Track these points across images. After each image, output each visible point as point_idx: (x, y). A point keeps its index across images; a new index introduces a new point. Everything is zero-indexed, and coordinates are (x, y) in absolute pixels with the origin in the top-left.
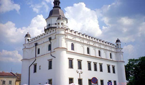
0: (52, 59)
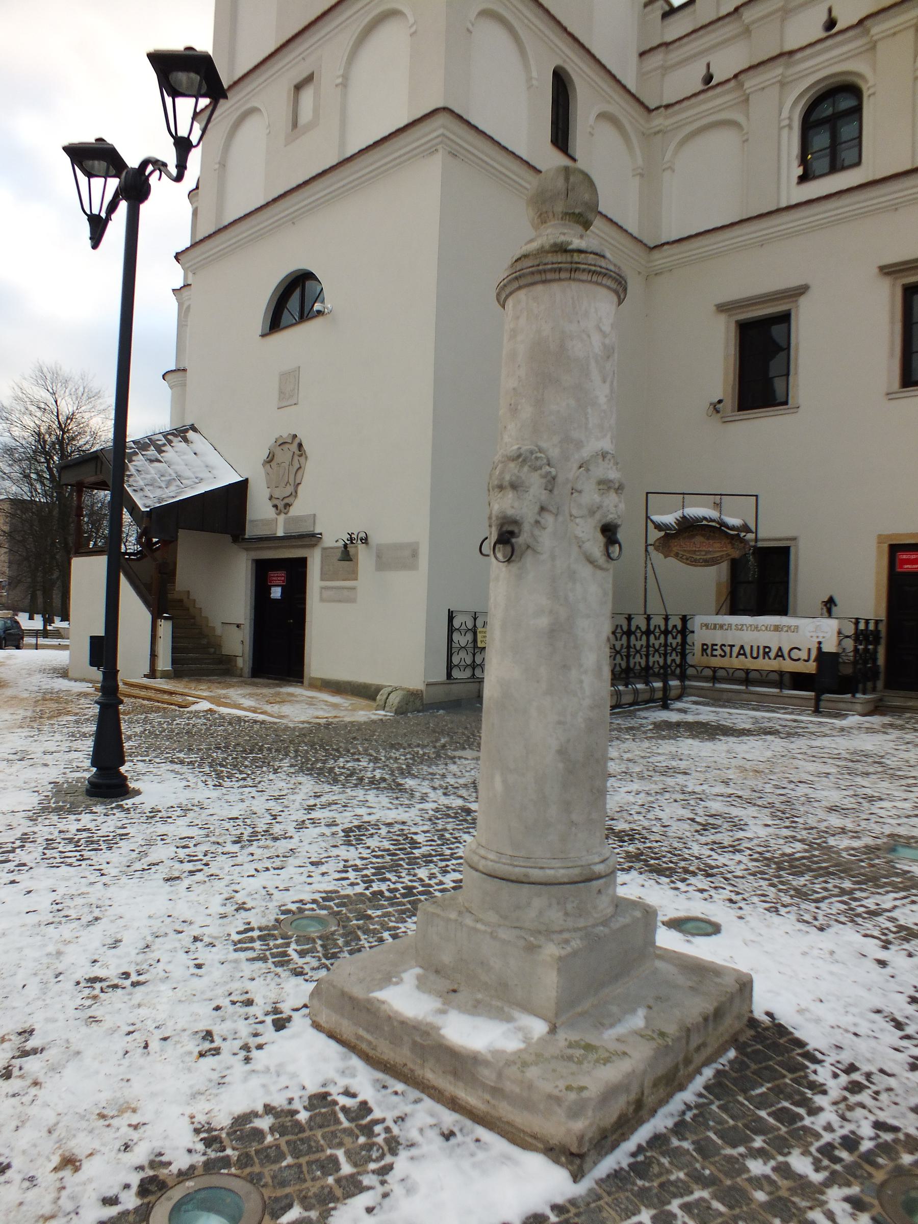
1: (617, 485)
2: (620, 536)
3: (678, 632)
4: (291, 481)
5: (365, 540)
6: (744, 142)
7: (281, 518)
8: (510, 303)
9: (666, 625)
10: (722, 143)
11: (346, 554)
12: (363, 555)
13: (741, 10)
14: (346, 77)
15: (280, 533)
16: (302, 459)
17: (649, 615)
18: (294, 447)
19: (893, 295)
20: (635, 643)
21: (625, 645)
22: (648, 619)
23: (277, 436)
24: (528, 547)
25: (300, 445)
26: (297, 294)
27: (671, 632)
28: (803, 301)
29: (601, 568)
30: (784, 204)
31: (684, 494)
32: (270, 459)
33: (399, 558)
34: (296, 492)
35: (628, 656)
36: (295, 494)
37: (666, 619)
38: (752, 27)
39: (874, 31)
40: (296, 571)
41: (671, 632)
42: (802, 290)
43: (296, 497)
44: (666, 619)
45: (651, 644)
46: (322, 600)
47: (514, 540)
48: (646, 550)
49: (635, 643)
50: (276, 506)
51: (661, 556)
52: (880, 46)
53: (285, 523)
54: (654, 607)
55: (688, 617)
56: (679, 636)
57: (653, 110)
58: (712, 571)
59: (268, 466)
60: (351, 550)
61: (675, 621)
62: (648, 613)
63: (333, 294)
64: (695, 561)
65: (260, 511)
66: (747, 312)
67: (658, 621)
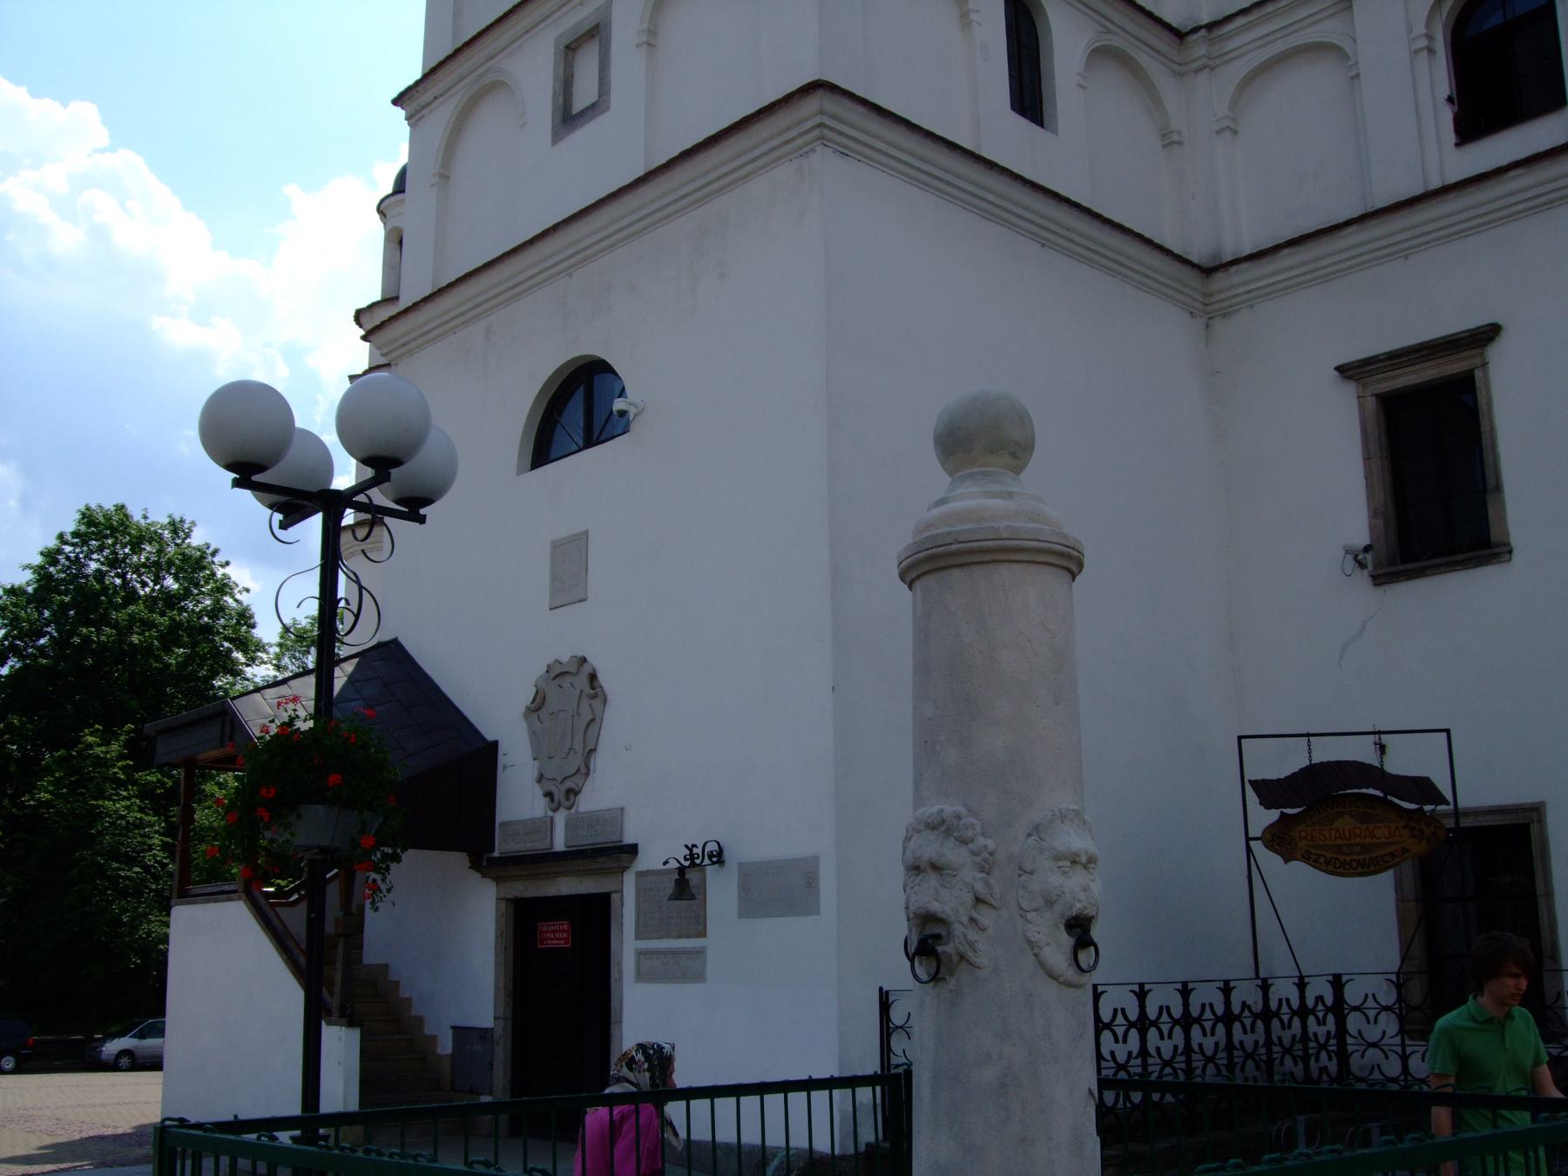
1: (1084, 859)
2: (1096, 933)
3: (1327, 1010)
4: (578, 746)
5: (718, 857)
6: (1352, 78)
7: (560, 818)
8: (917, 584)
9: (1302, 997)
10: (1311, 86)
11: (685, 883)
12: (721, 891)
14: (652, 32)
15: (559, 845)
16: (596, 703)
17: (1265, 980)
18: (582, 682)
20: (1243, 1037)
21: (1222, 1045)
22: (1265, 987)
23: (551, 661)
24: (962, 957)
25: (593, 677)
26: (579, 396)
27: (1313, 1011)
29: (1069, 985)
30: (1435, 183)
31: (1308, 735)
32: (537, 706)
33: (783, 889)
34: (588, 767)
35: (1231, 1066)
36: (586, 771)
37: (1301, 985)
40: (594, 916)
41: (1313, 1011)
42: (1490, 333)
43: (587, 774)
44: (1301, 985)
45: (1275, 1039)
46: (640, 976)
47: (940, 949)
48: (1249, 850)
49: (1243, 1037)
50: (549, 795)
51: (1278, 859)
53: (566, 826)
54: (1278, 964)
55: (1344, 979)
56: (1331, 1018)
57: (1188, 33)
58: (1386, 879)
59: (535, 716)
60: (692, 876)
61: (1319, 988)
62: (1262, 975)
63: (641, 384)
64: (1343, 864)
65: (519, 797)
66: (1396, 377)
67: (1284, 990)
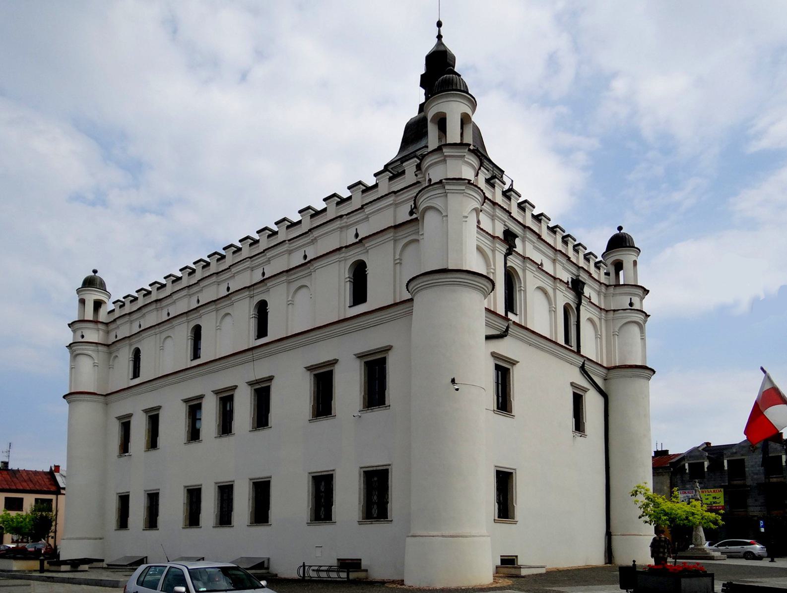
0: (589, 390)
13: (117, 320)
19: (361, 366)
28: (390, 353)
30: (398, 301)
38: (176, 301)
39: (268, 285)
42: (335, 362)
52: (369, 251)
